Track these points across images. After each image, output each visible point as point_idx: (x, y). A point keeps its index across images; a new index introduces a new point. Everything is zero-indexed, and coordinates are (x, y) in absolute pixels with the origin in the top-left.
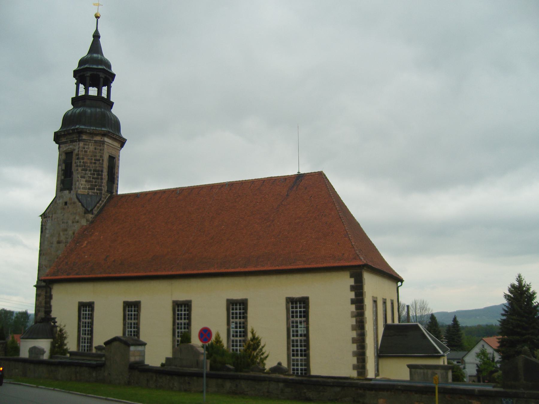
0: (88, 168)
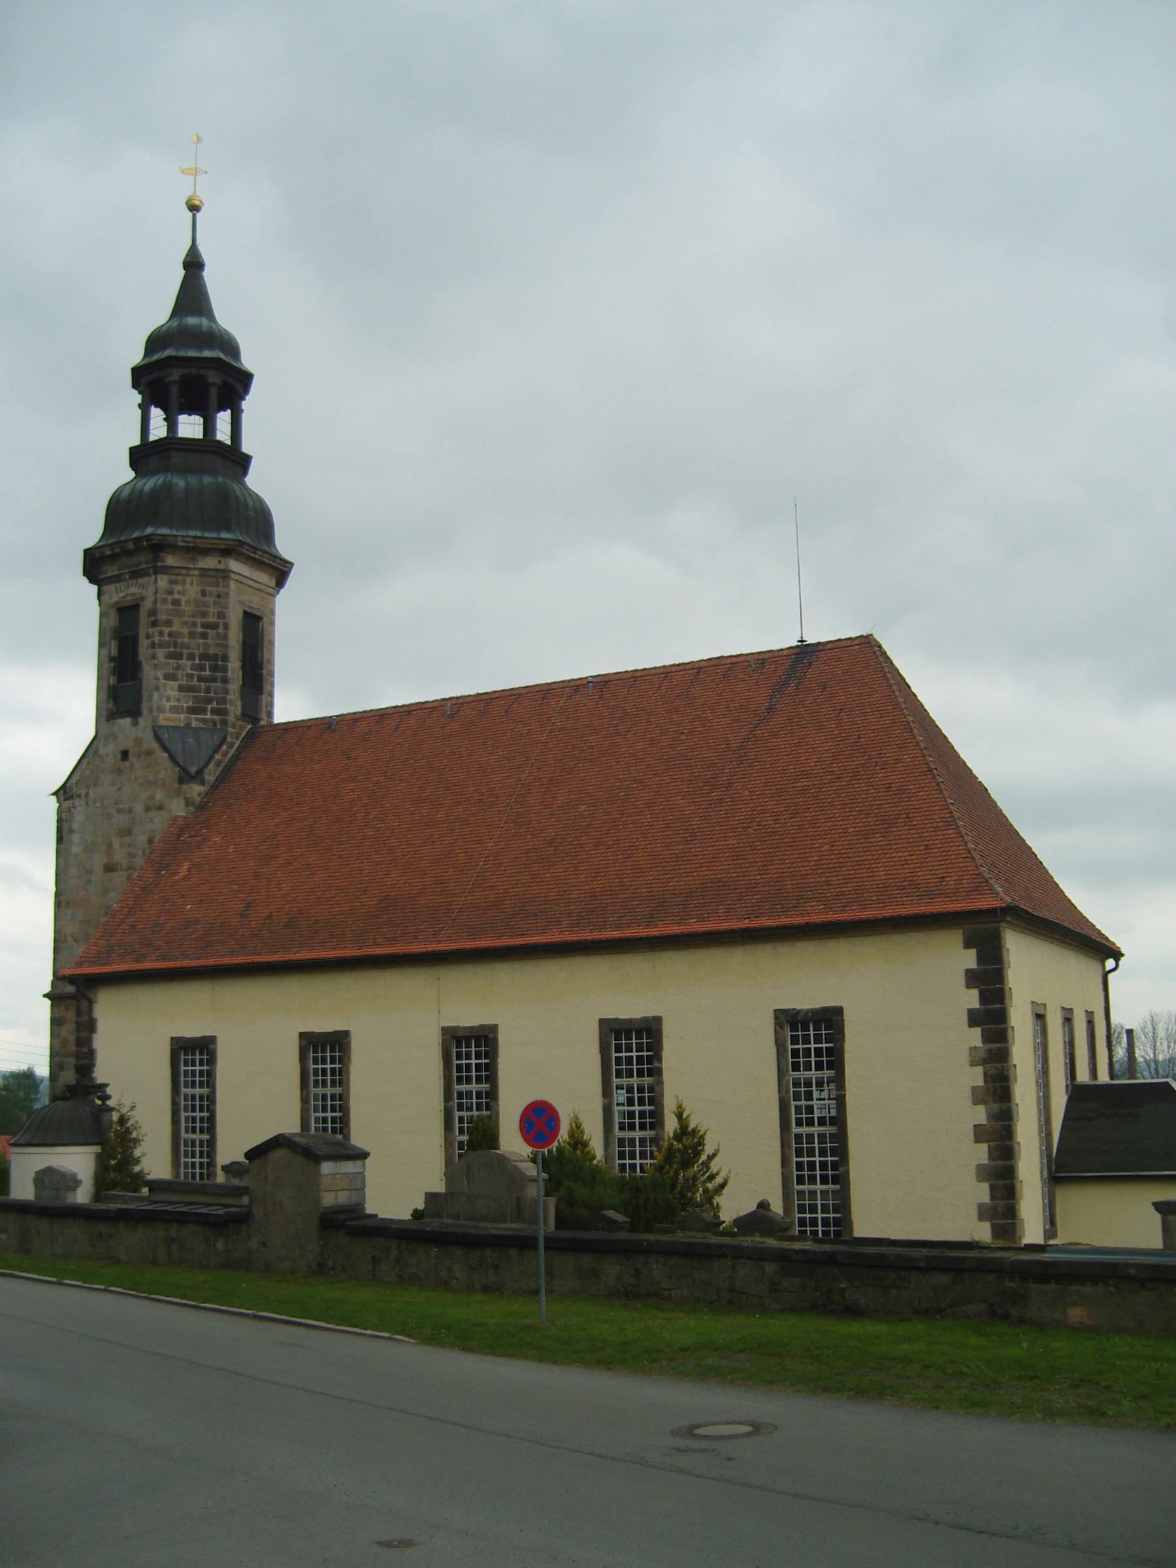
0: (185, 651)
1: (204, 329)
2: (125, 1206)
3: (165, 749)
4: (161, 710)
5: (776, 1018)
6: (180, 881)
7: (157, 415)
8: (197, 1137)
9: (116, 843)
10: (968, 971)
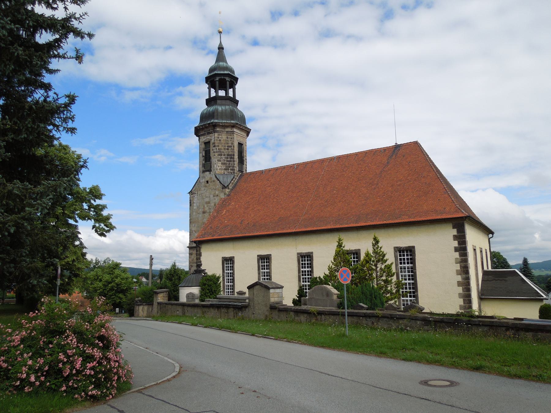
1: (225, 66)
2: (212, 303)
3: (218, 180)
4: (217, 169)
5: (394, 249)
6: (224, 215)
7: (213, 90)
8: (230, 284)
9: (206, 206)
10: (454, 235)
